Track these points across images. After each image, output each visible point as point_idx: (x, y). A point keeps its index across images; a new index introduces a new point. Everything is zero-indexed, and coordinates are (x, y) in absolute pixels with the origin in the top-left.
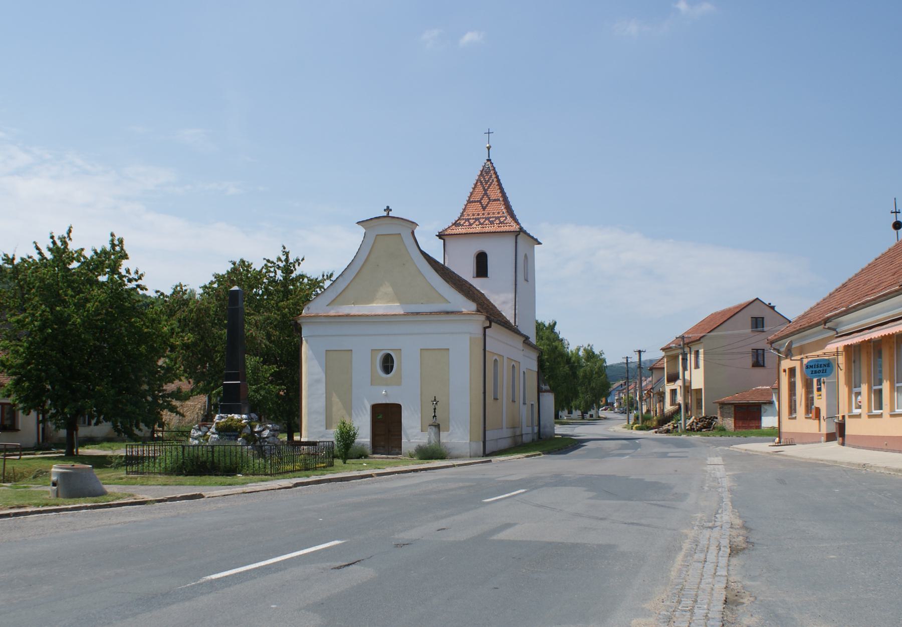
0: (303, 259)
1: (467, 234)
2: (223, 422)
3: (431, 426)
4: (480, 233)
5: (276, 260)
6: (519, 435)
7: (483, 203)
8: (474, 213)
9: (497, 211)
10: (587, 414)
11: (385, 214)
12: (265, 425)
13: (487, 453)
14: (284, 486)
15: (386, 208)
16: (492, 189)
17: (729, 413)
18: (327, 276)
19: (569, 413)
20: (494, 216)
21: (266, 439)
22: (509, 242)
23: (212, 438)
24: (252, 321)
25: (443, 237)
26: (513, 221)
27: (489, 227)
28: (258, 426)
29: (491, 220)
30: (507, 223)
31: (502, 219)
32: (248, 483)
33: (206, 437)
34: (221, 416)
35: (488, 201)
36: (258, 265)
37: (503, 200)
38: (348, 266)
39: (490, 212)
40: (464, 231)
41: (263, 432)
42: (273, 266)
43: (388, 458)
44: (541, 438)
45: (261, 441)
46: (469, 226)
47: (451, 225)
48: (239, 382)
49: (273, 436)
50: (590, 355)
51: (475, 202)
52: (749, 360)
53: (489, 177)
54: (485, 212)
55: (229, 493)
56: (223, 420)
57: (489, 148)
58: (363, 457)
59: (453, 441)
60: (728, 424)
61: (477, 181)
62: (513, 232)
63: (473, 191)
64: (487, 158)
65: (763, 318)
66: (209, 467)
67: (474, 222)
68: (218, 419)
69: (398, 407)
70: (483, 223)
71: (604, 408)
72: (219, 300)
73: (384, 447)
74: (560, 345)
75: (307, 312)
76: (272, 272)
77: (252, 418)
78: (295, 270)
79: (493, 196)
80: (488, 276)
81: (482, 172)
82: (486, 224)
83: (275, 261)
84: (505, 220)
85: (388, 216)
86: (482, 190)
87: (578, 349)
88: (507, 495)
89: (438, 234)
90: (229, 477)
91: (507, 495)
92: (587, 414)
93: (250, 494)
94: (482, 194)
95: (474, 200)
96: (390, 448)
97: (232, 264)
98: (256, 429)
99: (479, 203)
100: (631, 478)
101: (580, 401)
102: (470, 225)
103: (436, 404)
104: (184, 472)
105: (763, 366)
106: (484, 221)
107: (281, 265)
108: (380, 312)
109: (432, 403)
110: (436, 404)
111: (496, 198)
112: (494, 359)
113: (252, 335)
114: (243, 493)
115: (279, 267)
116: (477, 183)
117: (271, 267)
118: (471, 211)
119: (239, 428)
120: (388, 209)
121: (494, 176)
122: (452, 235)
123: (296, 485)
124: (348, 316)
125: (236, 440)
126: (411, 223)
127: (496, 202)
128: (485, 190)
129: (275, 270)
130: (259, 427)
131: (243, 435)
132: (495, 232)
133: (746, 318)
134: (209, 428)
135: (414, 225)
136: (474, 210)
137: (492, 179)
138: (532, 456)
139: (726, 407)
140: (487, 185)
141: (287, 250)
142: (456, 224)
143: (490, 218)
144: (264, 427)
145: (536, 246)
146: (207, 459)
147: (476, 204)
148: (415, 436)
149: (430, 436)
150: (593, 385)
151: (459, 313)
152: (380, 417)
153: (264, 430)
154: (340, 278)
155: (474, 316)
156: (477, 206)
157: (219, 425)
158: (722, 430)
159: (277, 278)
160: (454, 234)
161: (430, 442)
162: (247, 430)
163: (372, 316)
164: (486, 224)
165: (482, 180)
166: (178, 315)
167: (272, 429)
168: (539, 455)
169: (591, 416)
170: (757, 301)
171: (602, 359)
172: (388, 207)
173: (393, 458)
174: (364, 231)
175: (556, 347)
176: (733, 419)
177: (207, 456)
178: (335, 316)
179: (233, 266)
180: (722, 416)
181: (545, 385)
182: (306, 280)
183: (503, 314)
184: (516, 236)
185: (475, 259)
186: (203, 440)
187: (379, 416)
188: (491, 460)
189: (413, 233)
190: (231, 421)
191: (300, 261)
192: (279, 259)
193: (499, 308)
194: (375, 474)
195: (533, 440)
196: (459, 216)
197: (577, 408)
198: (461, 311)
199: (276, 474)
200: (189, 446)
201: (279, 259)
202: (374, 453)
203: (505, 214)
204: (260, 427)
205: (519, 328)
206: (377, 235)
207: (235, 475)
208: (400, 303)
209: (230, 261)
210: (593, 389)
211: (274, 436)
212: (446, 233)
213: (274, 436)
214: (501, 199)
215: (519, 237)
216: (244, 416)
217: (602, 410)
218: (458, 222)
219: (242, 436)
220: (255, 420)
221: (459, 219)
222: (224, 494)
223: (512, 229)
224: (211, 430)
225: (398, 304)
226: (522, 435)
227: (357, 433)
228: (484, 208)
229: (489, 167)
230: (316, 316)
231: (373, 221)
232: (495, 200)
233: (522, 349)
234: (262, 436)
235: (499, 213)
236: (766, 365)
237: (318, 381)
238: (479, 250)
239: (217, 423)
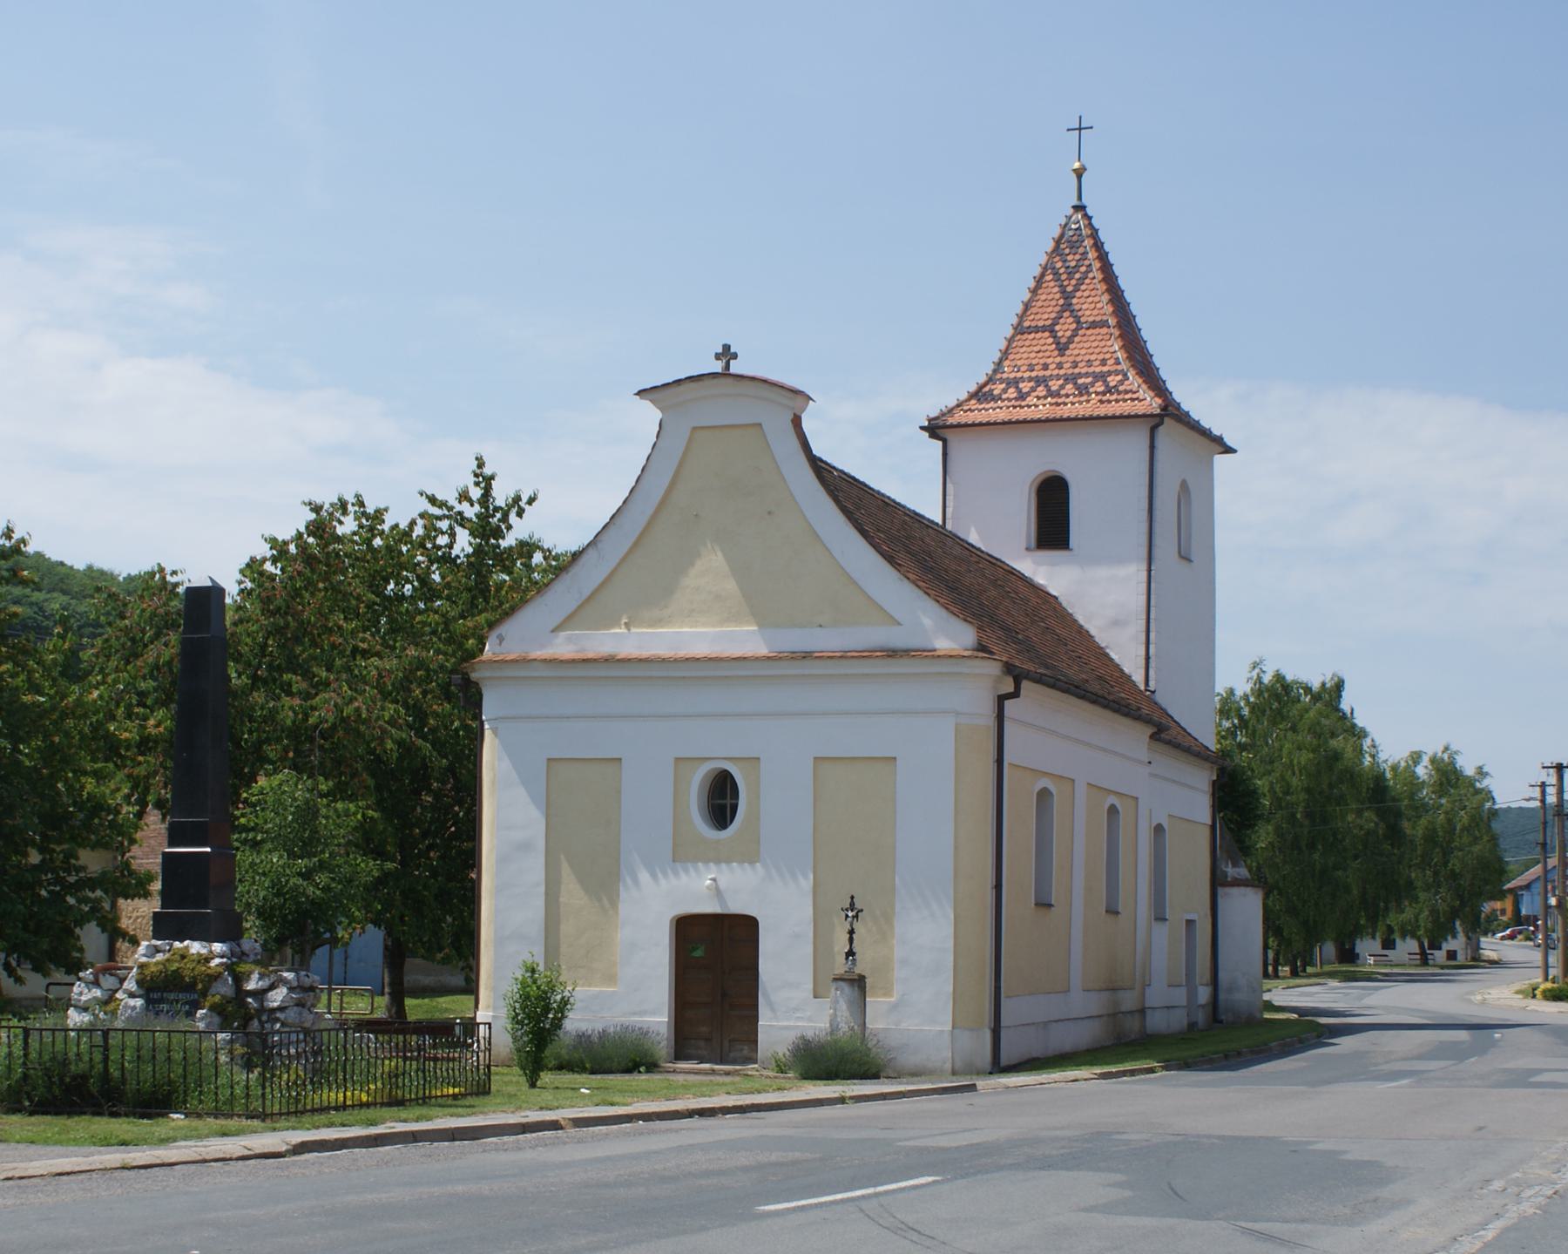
0: (531, 501)
1: (1010, 422)
2: (157, 963)
3: (841, 984)
4: (1047, 421)
6: (1131, 1012)
7: (1059, 334)
8: (1034, 362)
9: (1101, 357)
10: (1440, 949)
11: (718, 367)
12: (276, 971)
13: (1004, 1061)
14: (258, 1151)
15: (720, 350)
16: (1086, 294)
19: (1384, 947)
20: (1091, 370)
21: (278, 1015)
22: (1134, 444)
23: (126, 1006)
24: (369, 673)
25: (939, 432)
26: (1144, 386)
27: (1073, 404)
28: (255, 976)
29: (1080, 381)
30: (1126, 392)
31: (1113, 380)
32: (175, 1140)
33: (111, 1007)
34: (155, 946)
35: (1074, 326)
36: (402, 512)
37: (1119, 325)
39: (1078, 359)
40: (1001, 415)
42: (445, 517)
43: (713, 1072)
44: (1221, 1022)
45: (264, 1018)
46: (1016, 399)
47: (964, 396)
48: (208, 850)
49: (297, 1005)
50: (1448, 775)
51: (1037, 330)
53: (1077, 257)
54: (1064, 359)
55: (77, 1169)
56: (159, 957)
57: (1079, 173)
58: (642, 1069)
59: (903, 1026)
61: (1045, 269)
62: (1144, 416)
63: (1030, 300)
64: (1075, 202)
66: (94, 1090)
67: (1033, 390)
68: (144, 955)
69: (748, 926)
70: (1059, 390)
71: (1508, 932)
72: (273, 614)
73: (708, 1040)
74: (1349, 749)
75: (498, 649)
76: (443, 533)
77: (243, 953)
78: (509, 527)
79: (1088, 313)
80: (1071, 546)
81: (1058, 242)
82: (1067, 396)
83: (452, 502)
84: (1121, 382)
85: (726, 374)
86: (1058, 296)
87: (1416, 757)
88: (839, 1196)
89: (926, 424)
90: (145, 1121)
91: (839, 1196)
92: (1440, 949)
93: (143, 1171)
94: (1058, 308)
95: (1033, 324)
96: (726, 1043)
97: (312, 510)
98: (252, 985)
99: (1047, 334)
100: (1320, 1146)
101: (1417, 911)
102: (1022, 396)
103: (856, 916)
104: (27, 1103)
106: (1062, 387)
107: (470, 512)
108: (701, 649)
109: (843, 914)
110: (856, 916)
111: (1098, 319)
112: (1037, 789)
113: (360, 715)
114: (123, 1168)
115: (461, 520)
116: (1043, 275)
117: (439, 518)
118: (1025, 356)
119: (202, 981)
120: (727, 354)
121: (1092, 255)
122: (966, 425)
123: (301, 1148)
124: (609, 660)
125: (190, 1014)
126: (791, 395)
127: (1097, 331)
128: (1067, 296)
129: (451, 528)
130: (260, 979)
131: (210, 1000)
132: (1091, 418)
134: (122, 981)
135: (800, 399)
136: (1033, 355)
137: (1087, 262)
138: (1124, 1073)
140: (1073, 282)
141: (487, 471)
142: (980, 395)
143: (1080, 375)
144: (273, 978)
145: (1220, 461)
146: (92, 1067)
147: (1039, 335)
148: (796, 1010)
149: (835, 1010)
150: (1455, 863)
151: (928, 654)
152: (699, 953)
153: (272, 987)
155: (969, 662)
156: (1042, 341)
157: (147, 972)
159: (454, 553)
160: (973, 425)
161: (834, 1029)
162: (225, 988)
163: (676, 660)
164: (1067, 396)
165: (1059, 265)
166: (150, 656)
167: (295, 984)
168: (1151, 1070)
169: (1452, 955)
171: (1483, 789)
172: (727, 348)
173: (727, 1073)
174: (657, 415)
175: (1336, 756)
177: (91, 1059)
178: (573, 661)
179: (313, 516)
181: (1235, 865)
182: (538, 558)
183: (1113, 655)
184: (1153, 430)
185: (1034, 496)
186: (105, 1013)
187: (694, 949)
188: (975, 1085)
189: (797, 422)
190: (179, 962)
191: (522, 504)
192: (464, 496)
193: (1101, 637)
194: (570, 1119)
195: (1192, 1026)
196: (990, 372)
197: (1408, 931)
198: (930, 647)
199: (281, 1114)
200: (322, 1031)
201: (464, 496)
202: (680, 1054)
203: (1124, 366)
204: (262, 977)
205: (1159, 698)
206: (695, 429)
207: (165, 1115)
208: (761, 625)
209: (307, 501)
210: (1454, 876)
211: (300, 1004)
212: (951, 421)
213: (300, 1004)
214: (1112, 321)
215: (1161, 430)
216: (218, 947)
217: (1503, 938)
218: (986, 389)
219: (207, 1004)
220: (252, 957)
221: (990, 380)
222: (59, 1171)
223: (1139, 408)
224: (126, 985)
225: (756, 628)
226: (1142, 1011)
227: (572, 1000)
228: (1062, 348)
229: (1079, 229)
230: (524, 661)
231: (682, 388)
232: (1094, 325)
233: (1145, 758)
234: (265, 1004)
235: (1104, 362)
237: (525, 847)
238: (1052, 467)
239: (142, 966)
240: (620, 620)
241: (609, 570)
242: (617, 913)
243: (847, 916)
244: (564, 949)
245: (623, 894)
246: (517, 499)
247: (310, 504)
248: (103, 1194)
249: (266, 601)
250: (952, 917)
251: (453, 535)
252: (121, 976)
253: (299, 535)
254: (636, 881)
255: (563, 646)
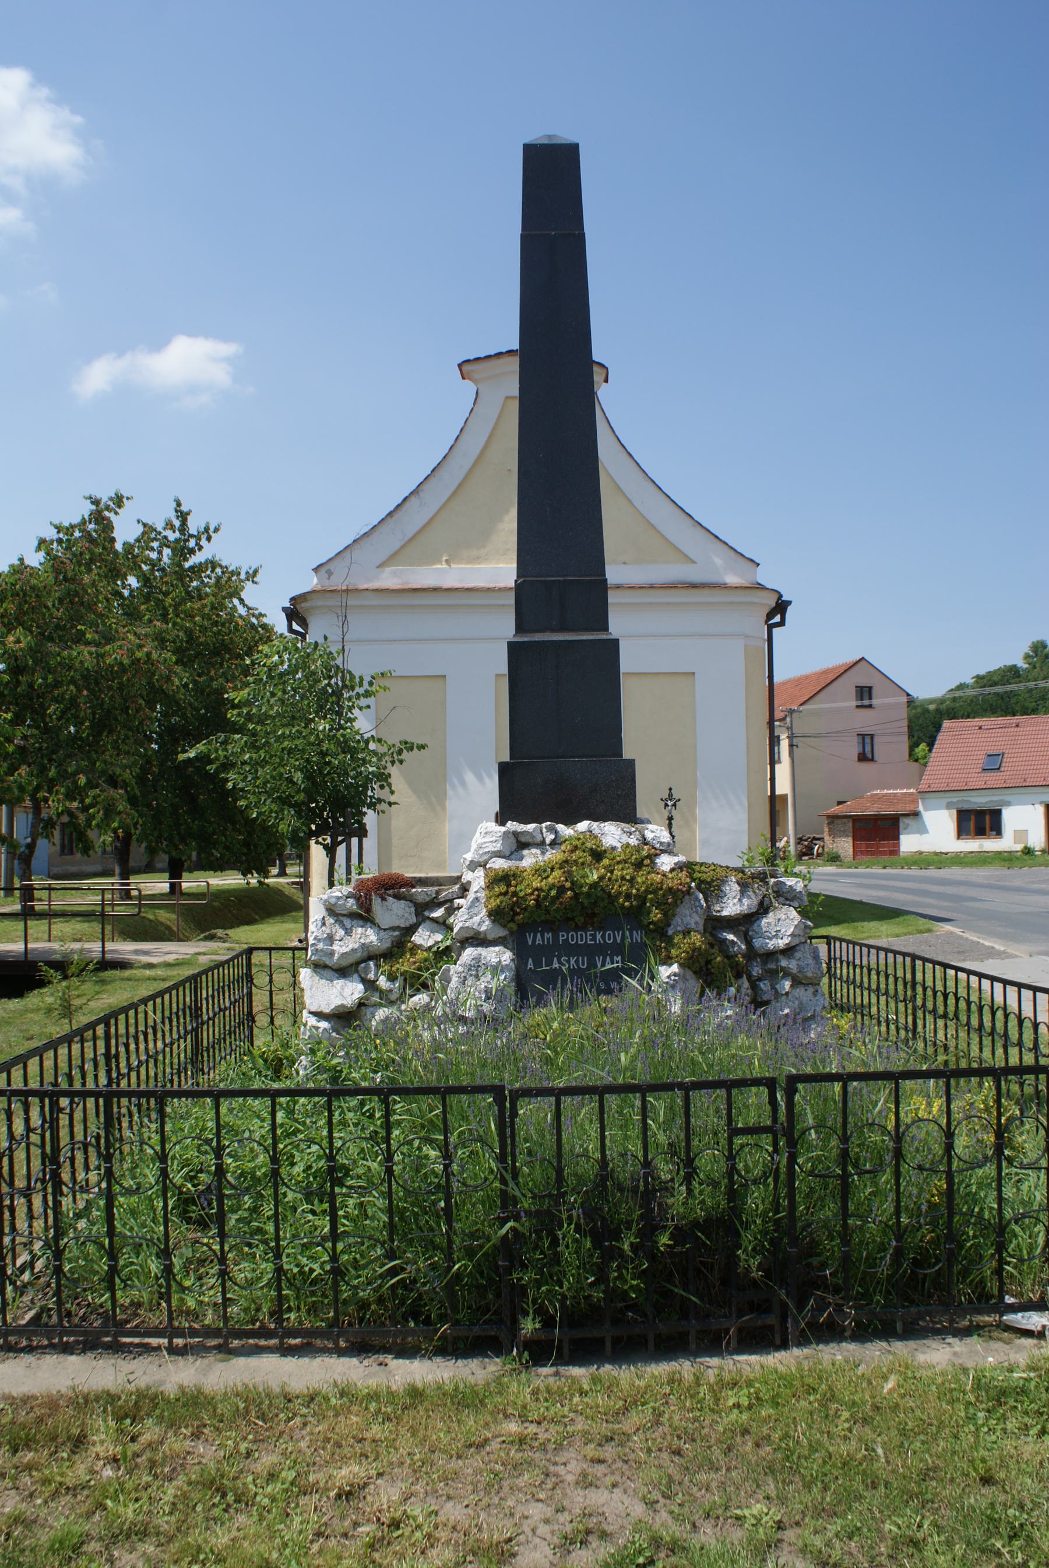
0: (216, 530)
5: (163, 525)
17: (844, 831)
18: (247, 573)
34: (516, 834)
38: (433, 471)
41: (767, 922)
52: (853, 749)
60: (843, 848)
65: (870, 688)
78: (200, 548)
103: (674, 805)
105: (872, 760)
109: (663, 803)
110: (674, 805)
130: (743, 893)
133: (848, 685)
139: (839, 821)
141: (184, 508)
154: (413, 499)
157: (523, 890)
158: (834, 859)
170: (863, 663)
176: (850, 840)
179: (94, 507)
180: (832, 833)
186: (392, 978)
192: (169, 525)
201: (169, 525)
209: (87, 495)
236: (876, 758)
240: (441, 557)
241: (431, 516)
242: (444, 808)
243: (666, 805)
244: (395, 841)
245: (450, 792)
246: (207, 530)
247: (91, 498)
248: (246, 1265)
249: (57, 571)
250: (746, 803)
251: (160, 553)
252: (420, 899)
253: (83, 522)
254: (463, 783)
255: (389, 579)
